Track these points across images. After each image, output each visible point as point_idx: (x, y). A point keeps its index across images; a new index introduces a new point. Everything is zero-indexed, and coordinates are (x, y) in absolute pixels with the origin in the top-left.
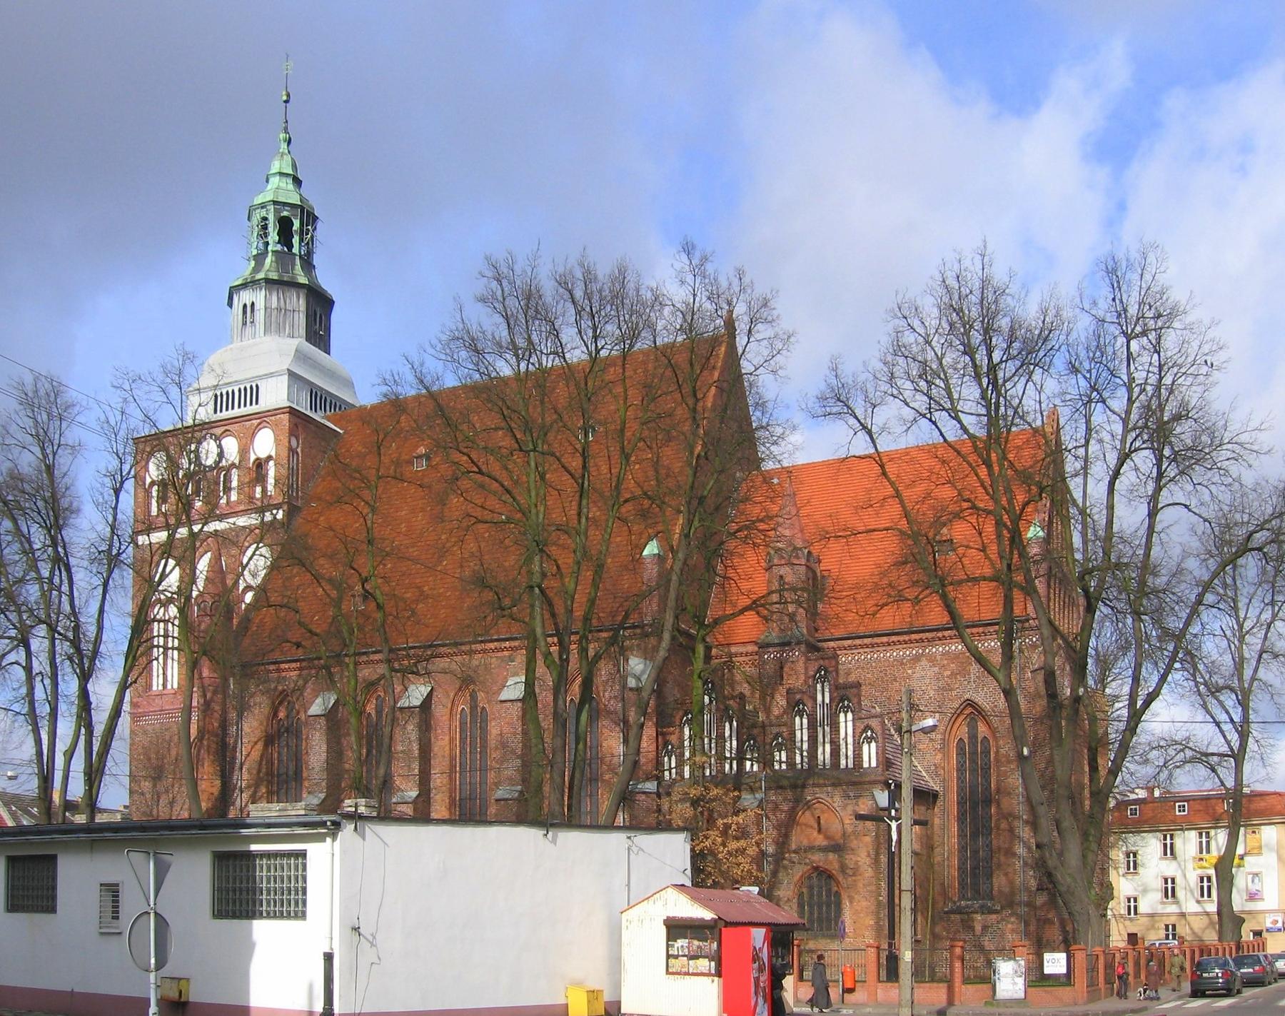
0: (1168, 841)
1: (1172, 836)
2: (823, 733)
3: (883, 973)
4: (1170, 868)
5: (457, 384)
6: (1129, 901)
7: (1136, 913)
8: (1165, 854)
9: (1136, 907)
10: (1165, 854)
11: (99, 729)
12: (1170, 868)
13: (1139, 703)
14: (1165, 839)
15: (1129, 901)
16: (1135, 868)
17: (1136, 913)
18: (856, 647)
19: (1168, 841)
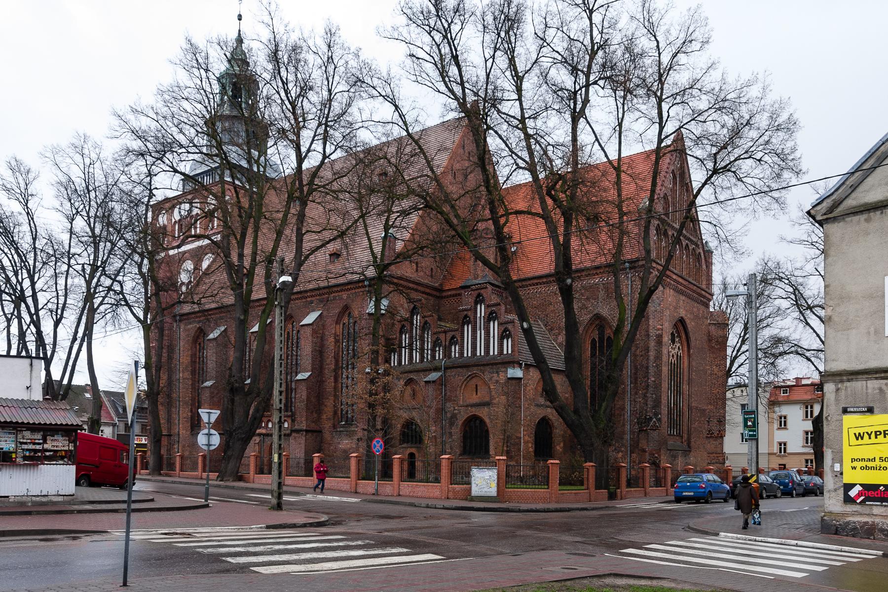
0: (809, 410)
1: (812, 407)
2: (481, 334)
3: (405, 474)
4: (780, 436)
5: (728, 271)
6: (780, 445)
7: (785, 452)
8: (807, 417)
9: (785, 449)
10: (807, 417)
11: (85, 344)
12: (780, 436)
13: (561, 239)
14: (807, 408)
15: (780, 445)
16: (785, 425)
17: (785, 452)
18: (537, 284)
19: (809, 410)
